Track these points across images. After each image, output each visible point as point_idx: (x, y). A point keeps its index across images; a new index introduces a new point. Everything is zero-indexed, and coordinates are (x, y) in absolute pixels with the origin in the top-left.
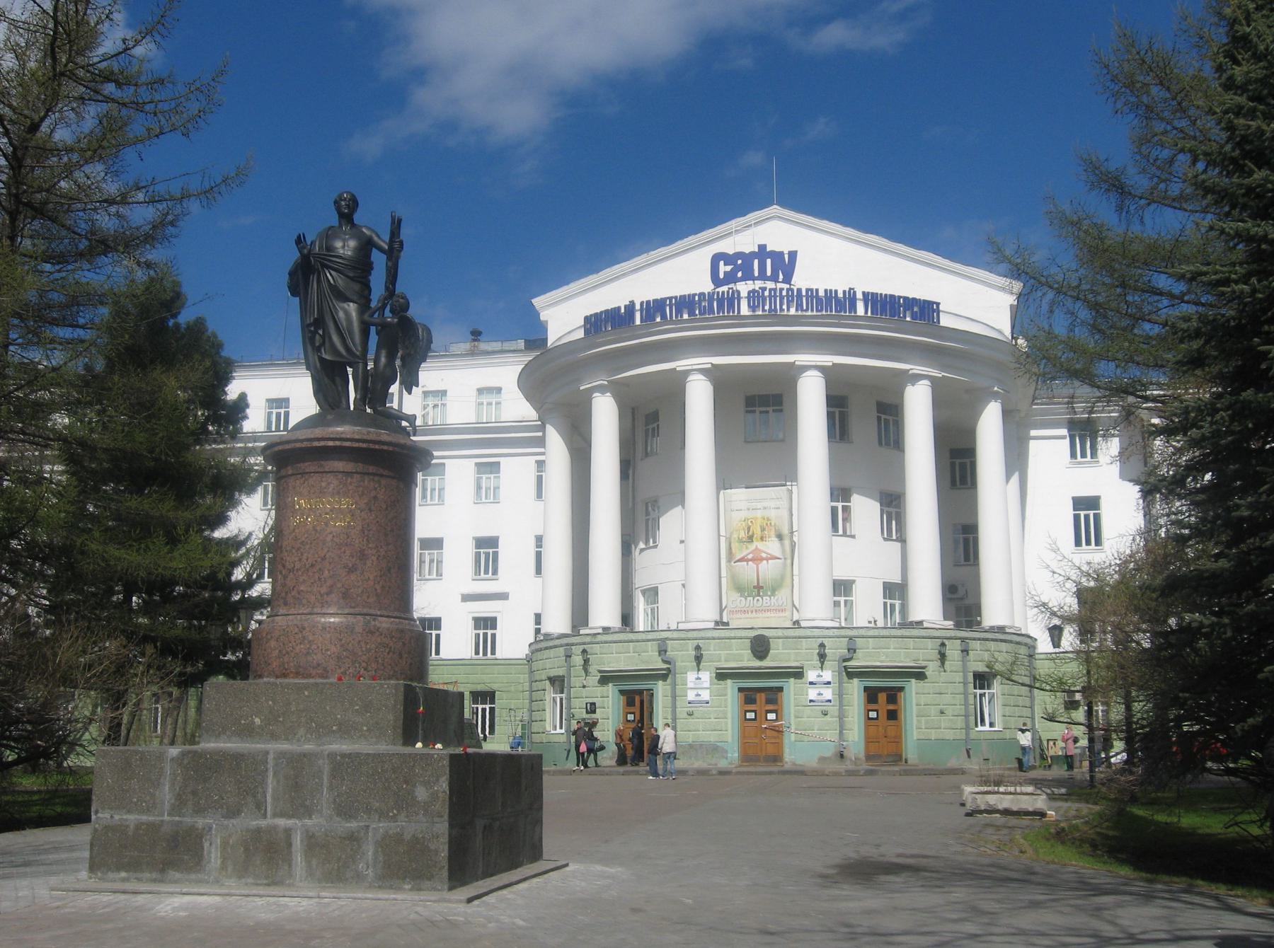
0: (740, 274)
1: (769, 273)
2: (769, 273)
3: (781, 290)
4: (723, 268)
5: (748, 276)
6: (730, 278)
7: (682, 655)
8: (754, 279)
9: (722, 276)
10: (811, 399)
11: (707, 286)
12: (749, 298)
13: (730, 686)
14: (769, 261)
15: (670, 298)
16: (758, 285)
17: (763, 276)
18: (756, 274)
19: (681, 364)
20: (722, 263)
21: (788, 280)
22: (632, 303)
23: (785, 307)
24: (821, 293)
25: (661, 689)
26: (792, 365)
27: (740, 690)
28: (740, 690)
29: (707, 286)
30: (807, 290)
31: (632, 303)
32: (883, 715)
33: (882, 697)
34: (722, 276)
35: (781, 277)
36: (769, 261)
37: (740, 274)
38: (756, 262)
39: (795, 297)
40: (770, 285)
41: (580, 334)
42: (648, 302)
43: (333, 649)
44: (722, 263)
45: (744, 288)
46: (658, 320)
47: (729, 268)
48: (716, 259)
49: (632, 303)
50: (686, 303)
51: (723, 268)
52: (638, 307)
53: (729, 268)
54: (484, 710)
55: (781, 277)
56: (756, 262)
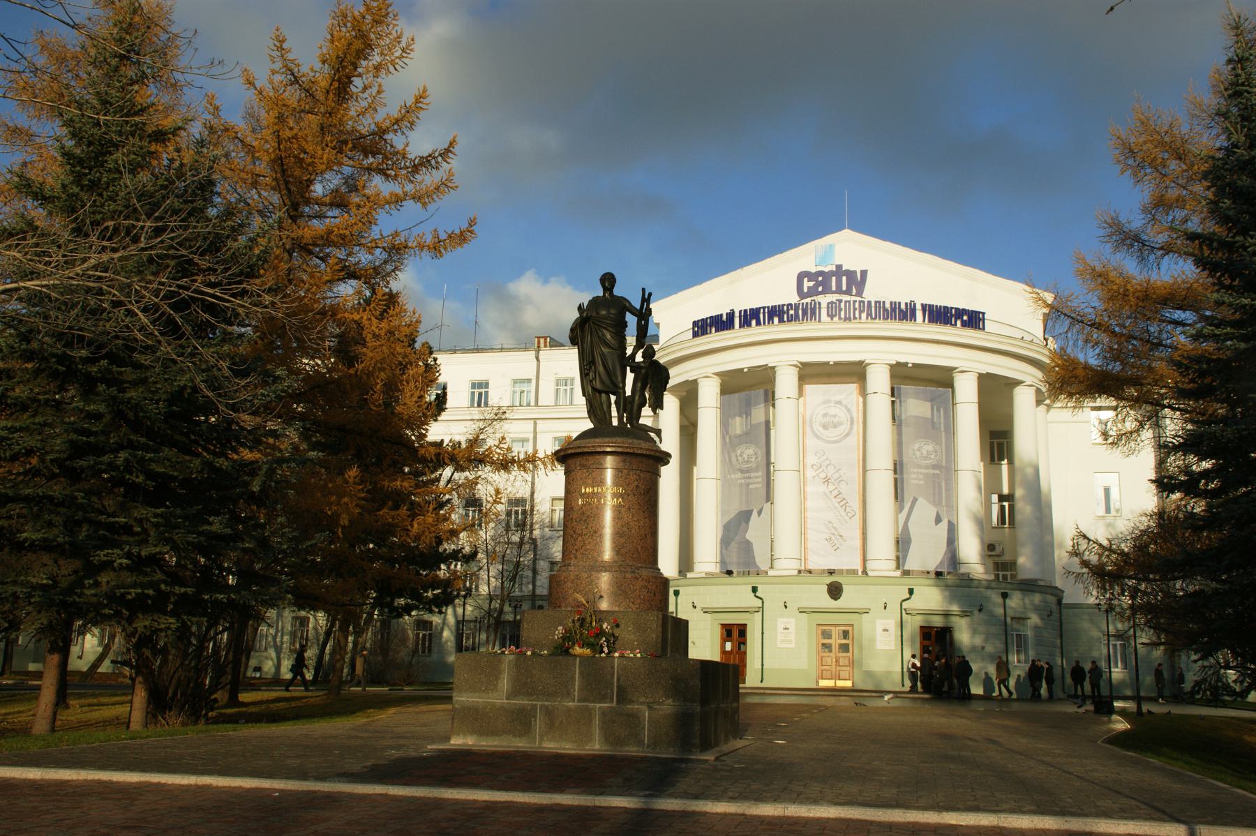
0: (820, 289)
1: (844, 288)
2: (844, 288)
5: (827, 290)
14: (844, 279)
17: (839, 291)
18: (834, 289)
21: (859, 294)
24: (888, 306)
36: (844, 279)
37: (820, 289)
40: (845, 298)
45: (824, 300)
47: (811, 284)
53: (811, 284)
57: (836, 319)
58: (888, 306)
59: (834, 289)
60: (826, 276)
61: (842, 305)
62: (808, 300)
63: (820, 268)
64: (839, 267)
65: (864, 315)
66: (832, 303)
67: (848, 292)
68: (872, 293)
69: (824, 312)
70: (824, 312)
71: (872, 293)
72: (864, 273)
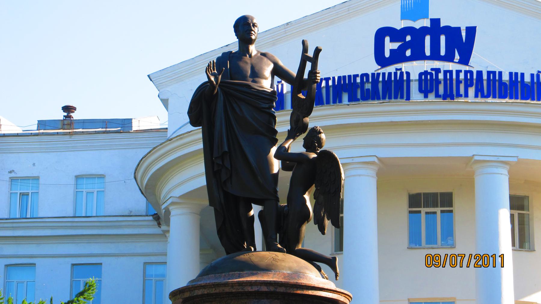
0: (408, 53)
1: (443, 52)
2: (443, 52)
5: (419, 55)
9: (387, 54)
14: (443, 38)
16: (427, 65)
17: (435, 56)
18: (428, 52)
21: (465, 60)
23: (462, 91)
24: (506, 78)
26: (468, 161)
36: (443, 38)
37: (408, 53)
38: (428, 39)
45: (415, 68)
47: (395, 46)
53: (395, 46)
56: (428, 39)
58: (506, 78)
59: (428, 52)
60: (418, 34)
61: (441, 76)
63: (408, 23)
64: (435, 22)
65: (472, 91)
66: (426, 73)
67: (449, 58)
68: (482, 60)
69: (414, 87)
70: (414, 87)
71: (482, 60)
72: (471, 31)
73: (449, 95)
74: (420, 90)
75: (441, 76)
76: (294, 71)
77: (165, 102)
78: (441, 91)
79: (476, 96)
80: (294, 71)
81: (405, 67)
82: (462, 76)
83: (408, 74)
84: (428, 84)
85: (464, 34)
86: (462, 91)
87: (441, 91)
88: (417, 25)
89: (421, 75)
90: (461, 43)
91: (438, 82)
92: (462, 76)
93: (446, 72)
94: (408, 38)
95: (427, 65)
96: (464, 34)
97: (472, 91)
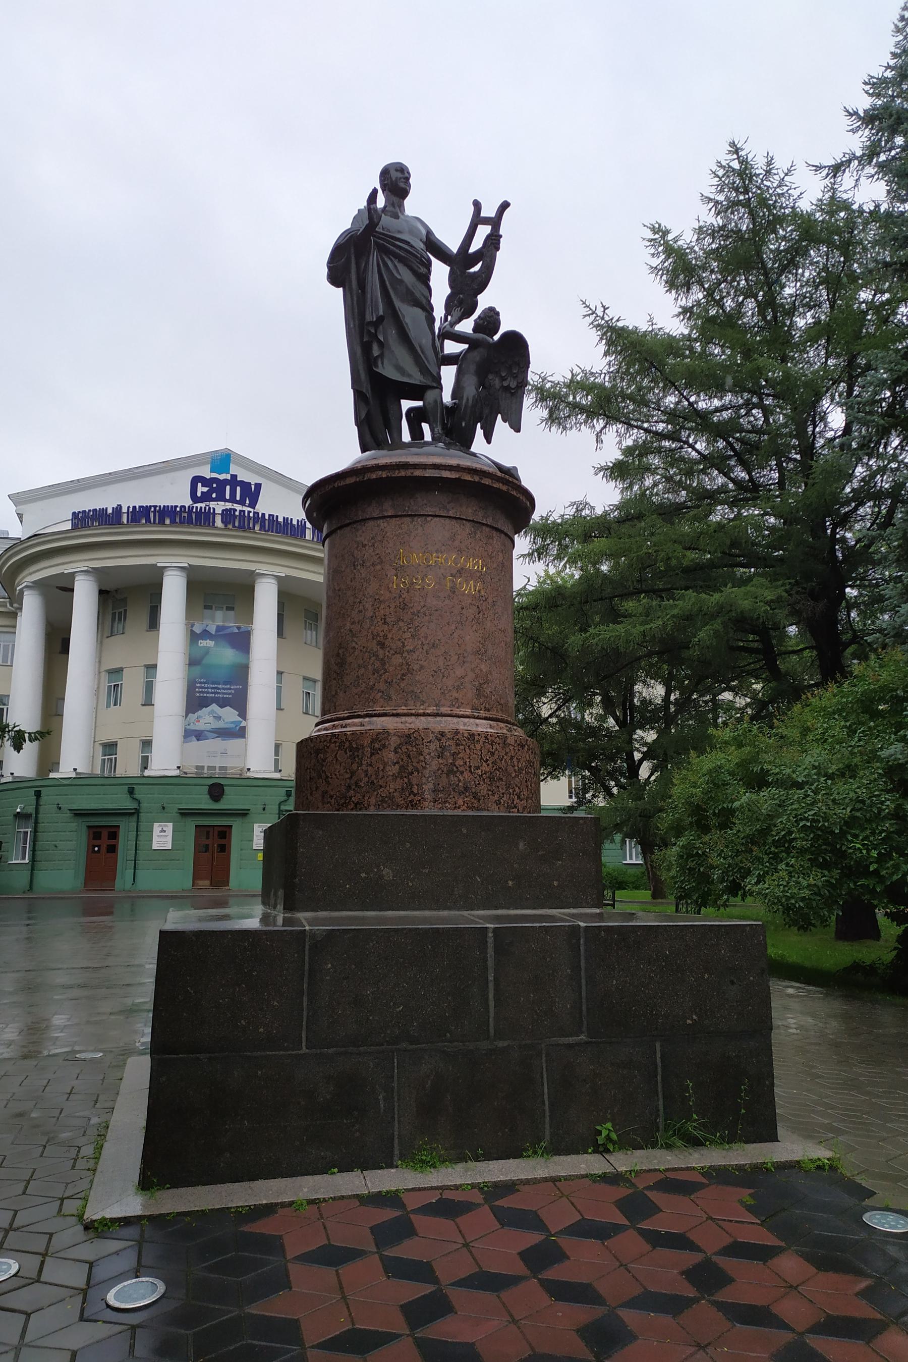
0: (214, 495)
1: (238, 498)
2: (238, 498)
3: (249, 512)
4: (201, 489)
5: (221, 498)
6: (206, 497)
7: (148, 799)
8: (226, 501)
9: (199, 494)
10: (174, 592)
11: (186, 501)
12: (222, 514)
13: (190, 825)
14: (238, 488)
15: (155, 507)
16: (229, 505)
17: (233, 500)
18: (228, 497)
19: (159, 558)
20: (200, 485)
21: (253, 505)
22: (120, 507)
23: (251, 525)
24: (281, 519)
25: (126, 830)
26: (252, 573)
27: (89, 827)
28: (89, 827)
29: (186, 501)
30: (270, 515)
31: (120, 507)
32: (104, 849)
33: (105, 834)
34: (199, 494)
35: (248, 502)
36: (238, 488)
37: (214, 495)
38: (228, 488)
39: (259, 519)
40: (238, 507)
41: (68, 526)
42: (134, 507)
43: (485, 767)
44: (200, 485)
45: (219, 507)
46: (144, 521)
47: (205, 489)
48: (196, 480)
49: (120, 506)
50: (166, 514)
51: (201, 489)
52: (125, 510)
53: (205, 489)
54: (631, 859)
55: (248, 502)
56: (228, 488)
57: (230, 526)
59: (228, 497)
60: (222, 484)
61: (237, 513)
62: (203, 505)
63: (214, 475)
64: (234, 477)
65: (257, 528)
68: (265, 506)
69: (218, 519)
70: (218, 519)
72: (258, 486)
73: (242, 527)
74: (222, 521)
75: (237, 513)
76: (454, 246)
77: (20, 516)
78: (237, 524)
79: (260, 530)
80: (454, 246)
81: (213, 504)
82: (251, 515)
83: (214, 509)
84: (228, 516)
85: (253, 487)
86: (251, 525)
87: (237, 524)
88: (222, 477)
89: (223, 511)
90: (251, 493)
91: (235, 517)
92: (251, 515)
93: (240, 511)
94: (215, 485)
95: (229, 505)
96: (253, 487)
97: (257, 528)
